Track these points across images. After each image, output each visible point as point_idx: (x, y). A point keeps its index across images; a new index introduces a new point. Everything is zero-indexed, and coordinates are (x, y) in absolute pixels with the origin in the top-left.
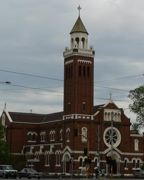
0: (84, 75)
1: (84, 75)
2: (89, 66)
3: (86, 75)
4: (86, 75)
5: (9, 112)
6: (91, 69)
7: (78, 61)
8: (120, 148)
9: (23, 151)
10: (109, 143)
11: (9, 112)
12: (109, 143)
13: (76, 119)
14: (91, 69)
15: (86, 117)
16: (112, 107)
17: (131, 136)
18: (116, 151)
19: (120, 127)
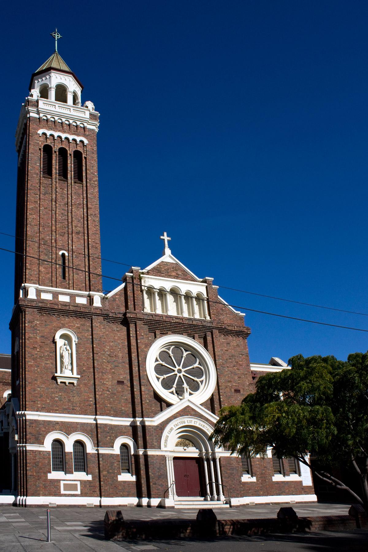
0: (64, 173)
1: (64, 173)
2: (82, 151)
3: (71, 174)
4: (71, 174)
5: (177, 445)
6: (85, 158)
7: (40, 132)
8: (217, 405)
9: (228, 457)
10: (173, 389)
11: (177, 445)
12: (173, 389)
13: (32, 300)
14: (85, 158)
15: (73, 297)
16: (174, 274)
17: (252, 369)
18: (201, 417)
19: (209, 338)
